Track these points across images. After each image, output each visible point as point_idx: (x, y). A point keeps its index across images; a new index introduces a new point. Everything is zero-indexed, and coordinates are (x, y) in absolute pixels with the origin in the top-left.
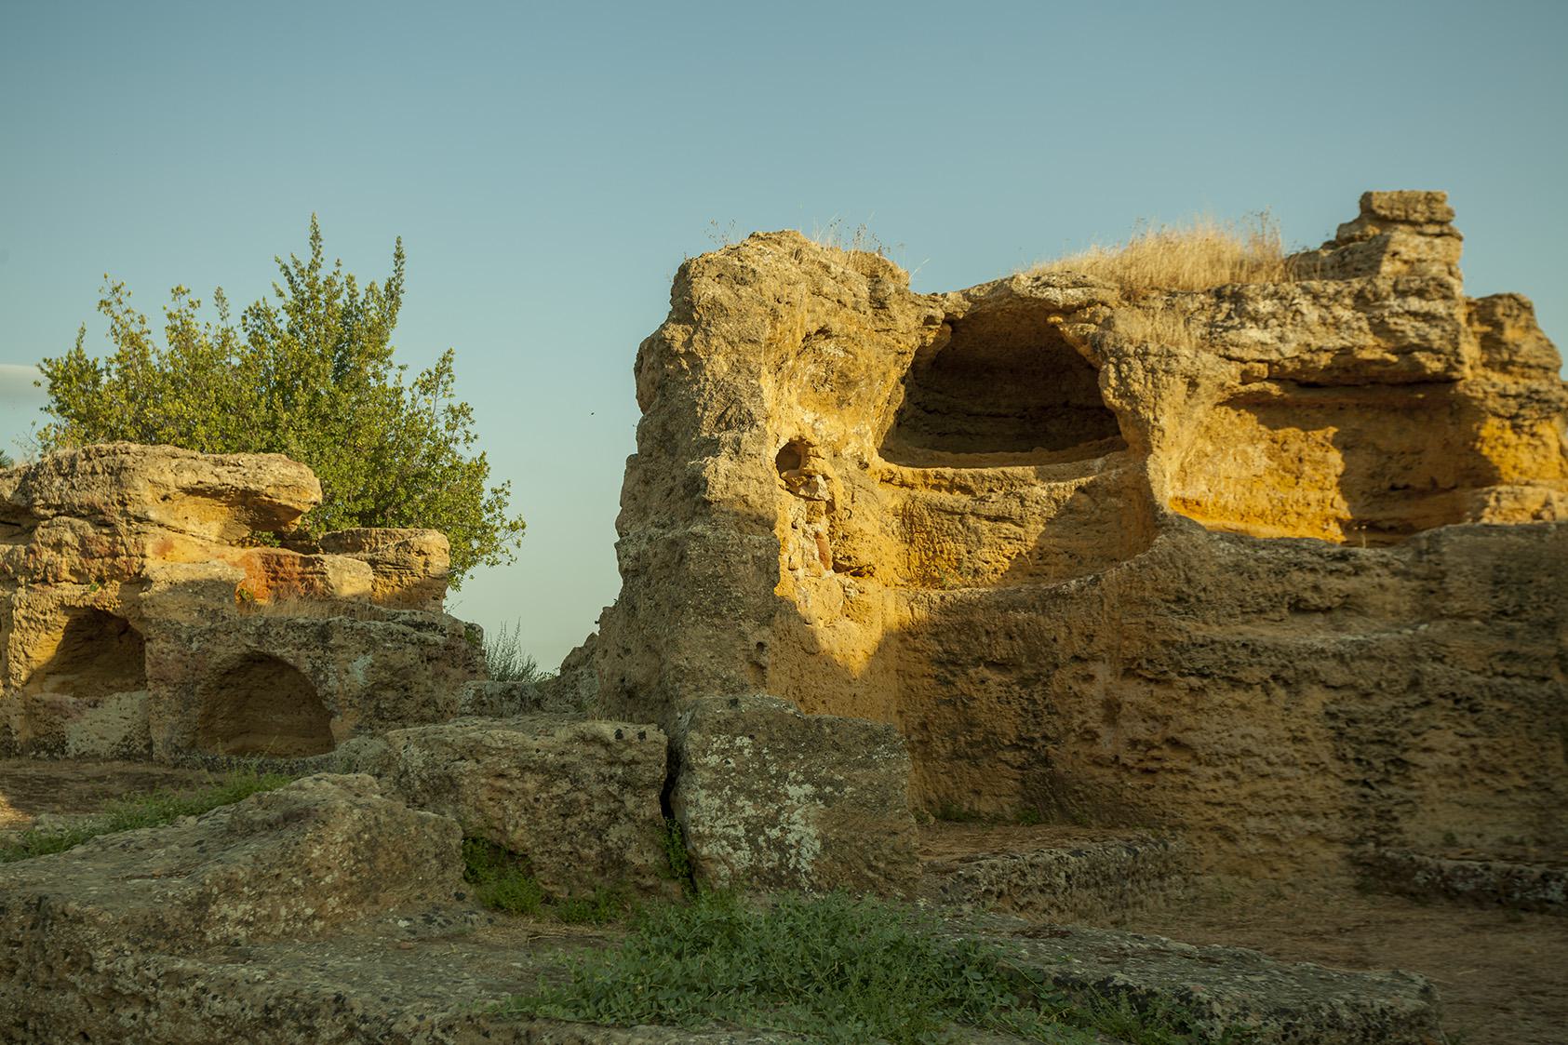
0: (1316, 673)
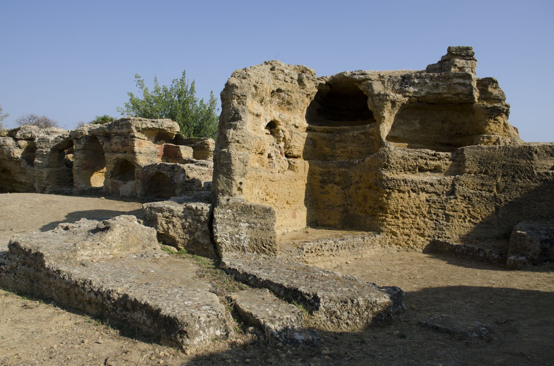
0: (424, 188)
